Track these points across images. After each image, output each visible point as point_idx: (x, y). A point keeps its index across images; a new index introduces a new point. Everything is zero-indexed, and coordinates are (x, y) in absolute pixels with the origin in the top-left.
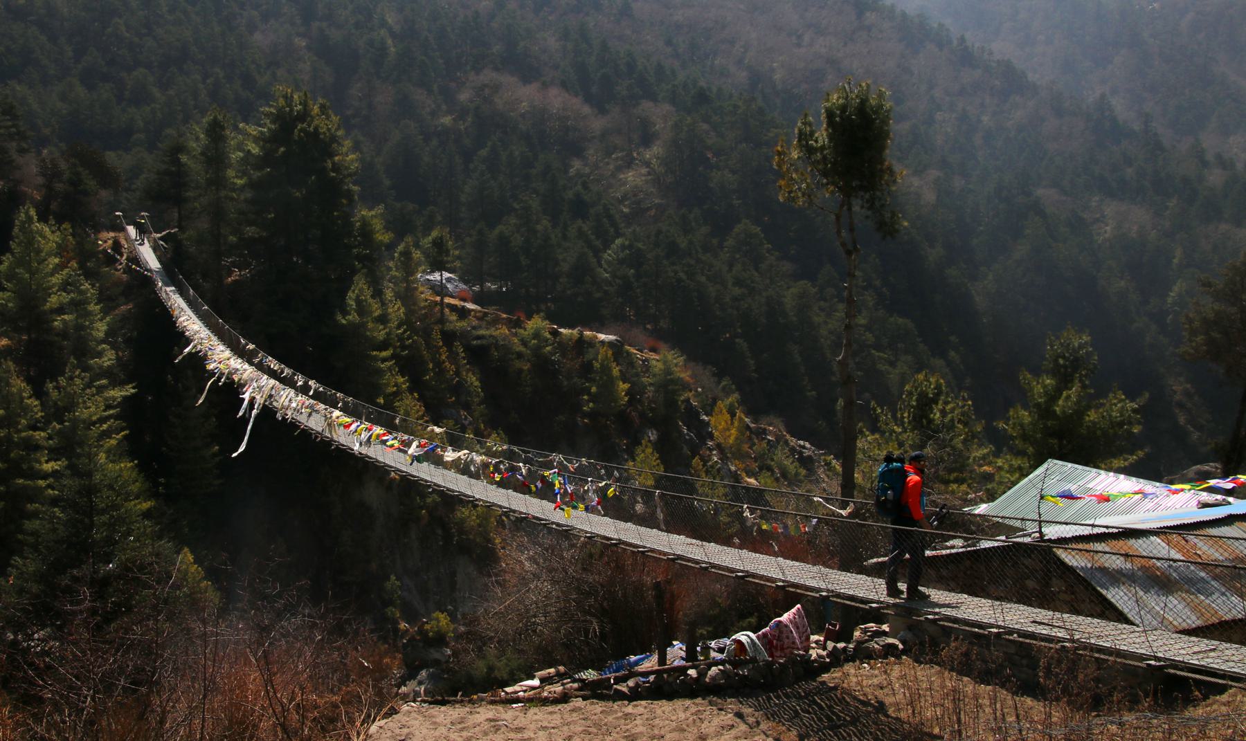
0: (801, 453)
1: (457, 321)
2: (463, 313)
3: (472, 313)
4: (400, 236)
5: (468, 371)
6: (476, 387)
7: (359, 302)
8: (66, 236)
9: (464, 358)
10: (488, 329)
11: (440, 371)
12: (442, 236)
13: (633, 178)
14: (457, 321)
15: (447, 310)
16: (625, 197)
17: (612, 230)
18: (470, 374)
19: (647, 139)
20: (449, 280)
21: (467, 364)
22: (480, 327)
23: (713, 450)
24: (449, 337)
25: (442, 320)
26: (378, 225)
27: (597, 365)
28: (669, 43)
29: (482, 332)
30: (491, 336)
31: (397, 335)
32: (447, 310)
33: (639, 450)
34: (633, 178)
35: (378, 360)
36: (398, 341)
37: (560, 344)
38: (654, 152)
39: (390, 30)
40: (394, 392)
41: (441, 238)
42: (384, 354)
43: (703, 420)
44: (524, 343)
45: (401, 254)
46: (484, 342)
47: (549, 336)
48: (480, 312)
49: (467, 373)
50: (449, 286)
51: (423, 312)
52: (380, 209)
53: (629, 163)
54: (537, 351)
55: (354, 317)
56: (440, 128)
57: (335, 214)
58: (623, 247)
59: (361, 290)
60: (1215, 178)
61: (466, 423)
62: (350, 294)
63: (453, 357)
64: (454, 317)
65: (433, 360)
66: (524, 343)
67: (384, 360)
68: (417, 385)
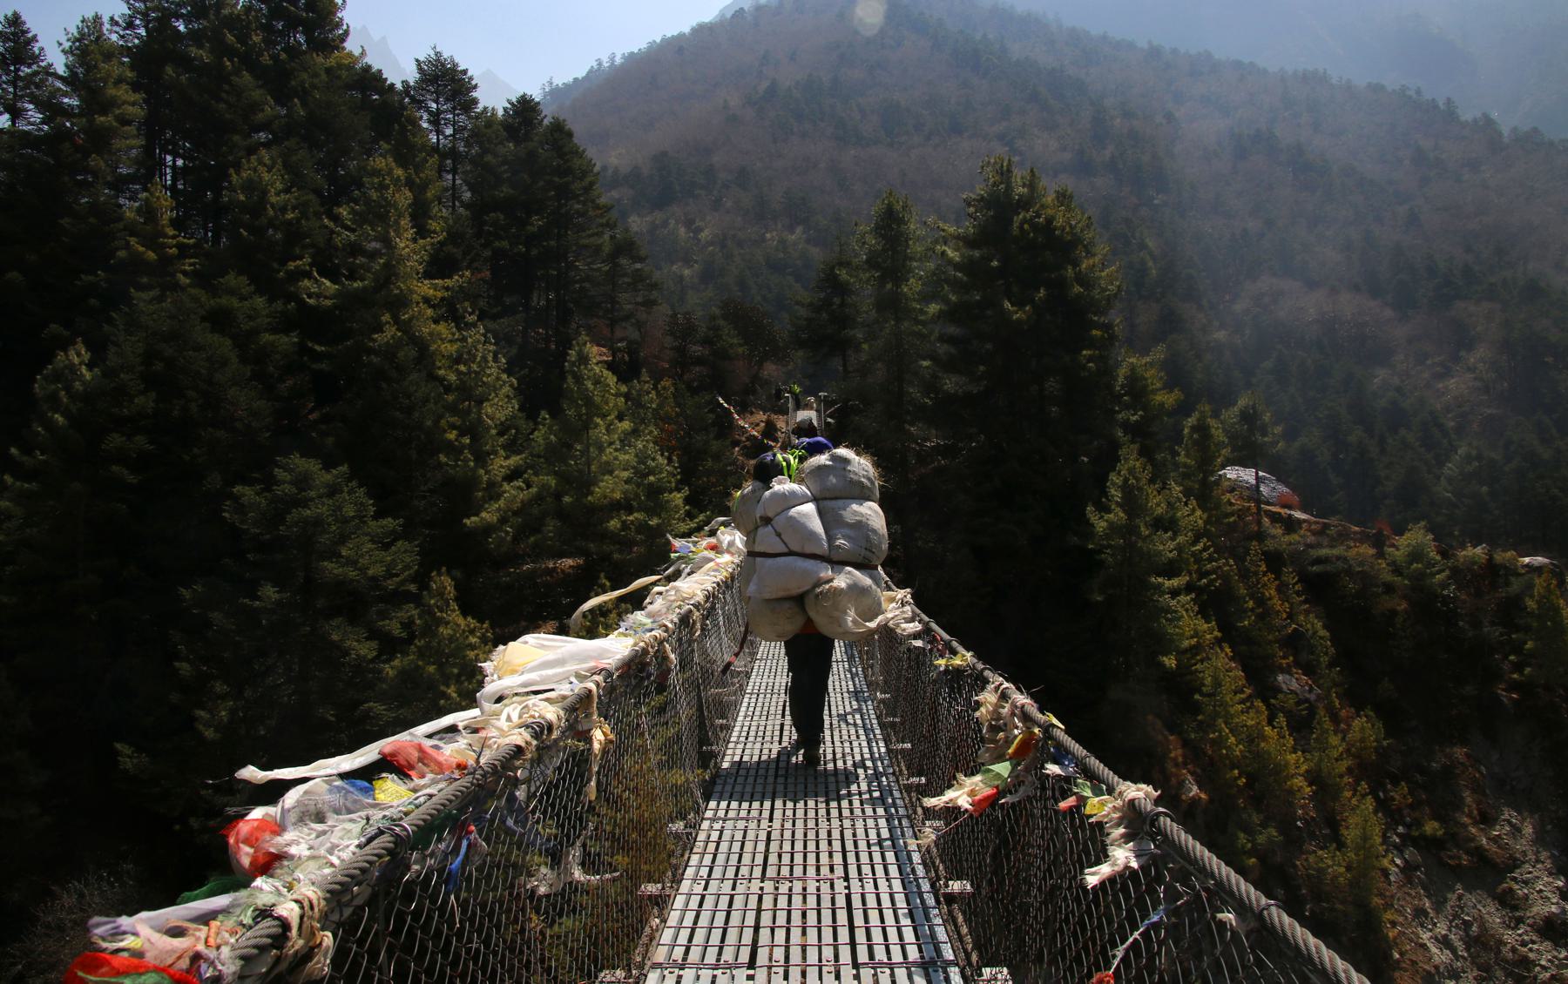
1: (1284, 534)
2: (1290, 525)
3: (1304, 525)
5: (1307, 612)
6: (1321, 638)
7: (1126, 488)
9: (1298, 594)
10: (1332, 547)
11: (1265, 613)
14: (1284, 534)
15: (1266, 521)
21: (1305, 602)
24: (1275, 561)
25: (1260, 536)
26: (1153, 377)
27: (1531, 604)
29: (1324, 552)
30: (1338, 558)
31: (1193, 554)
32: (1266, 521)
34: (1457, 385)
35: (1164, 593)
38: (1479, 356)
40: (1192, 648)
42: (1175, 582)
44: (1397, 570)
45: (1194, 429)
46: (1329, 568)
48: (1317, 523)
51: (1232, 519)
53: (1446, 373)
59: (1131, 471)
61: (1312, 697)
62: (1113, 477)
64: (1277, 531)
65: (1252, 597)
67: (1175, 593)
68: (1229, 633)
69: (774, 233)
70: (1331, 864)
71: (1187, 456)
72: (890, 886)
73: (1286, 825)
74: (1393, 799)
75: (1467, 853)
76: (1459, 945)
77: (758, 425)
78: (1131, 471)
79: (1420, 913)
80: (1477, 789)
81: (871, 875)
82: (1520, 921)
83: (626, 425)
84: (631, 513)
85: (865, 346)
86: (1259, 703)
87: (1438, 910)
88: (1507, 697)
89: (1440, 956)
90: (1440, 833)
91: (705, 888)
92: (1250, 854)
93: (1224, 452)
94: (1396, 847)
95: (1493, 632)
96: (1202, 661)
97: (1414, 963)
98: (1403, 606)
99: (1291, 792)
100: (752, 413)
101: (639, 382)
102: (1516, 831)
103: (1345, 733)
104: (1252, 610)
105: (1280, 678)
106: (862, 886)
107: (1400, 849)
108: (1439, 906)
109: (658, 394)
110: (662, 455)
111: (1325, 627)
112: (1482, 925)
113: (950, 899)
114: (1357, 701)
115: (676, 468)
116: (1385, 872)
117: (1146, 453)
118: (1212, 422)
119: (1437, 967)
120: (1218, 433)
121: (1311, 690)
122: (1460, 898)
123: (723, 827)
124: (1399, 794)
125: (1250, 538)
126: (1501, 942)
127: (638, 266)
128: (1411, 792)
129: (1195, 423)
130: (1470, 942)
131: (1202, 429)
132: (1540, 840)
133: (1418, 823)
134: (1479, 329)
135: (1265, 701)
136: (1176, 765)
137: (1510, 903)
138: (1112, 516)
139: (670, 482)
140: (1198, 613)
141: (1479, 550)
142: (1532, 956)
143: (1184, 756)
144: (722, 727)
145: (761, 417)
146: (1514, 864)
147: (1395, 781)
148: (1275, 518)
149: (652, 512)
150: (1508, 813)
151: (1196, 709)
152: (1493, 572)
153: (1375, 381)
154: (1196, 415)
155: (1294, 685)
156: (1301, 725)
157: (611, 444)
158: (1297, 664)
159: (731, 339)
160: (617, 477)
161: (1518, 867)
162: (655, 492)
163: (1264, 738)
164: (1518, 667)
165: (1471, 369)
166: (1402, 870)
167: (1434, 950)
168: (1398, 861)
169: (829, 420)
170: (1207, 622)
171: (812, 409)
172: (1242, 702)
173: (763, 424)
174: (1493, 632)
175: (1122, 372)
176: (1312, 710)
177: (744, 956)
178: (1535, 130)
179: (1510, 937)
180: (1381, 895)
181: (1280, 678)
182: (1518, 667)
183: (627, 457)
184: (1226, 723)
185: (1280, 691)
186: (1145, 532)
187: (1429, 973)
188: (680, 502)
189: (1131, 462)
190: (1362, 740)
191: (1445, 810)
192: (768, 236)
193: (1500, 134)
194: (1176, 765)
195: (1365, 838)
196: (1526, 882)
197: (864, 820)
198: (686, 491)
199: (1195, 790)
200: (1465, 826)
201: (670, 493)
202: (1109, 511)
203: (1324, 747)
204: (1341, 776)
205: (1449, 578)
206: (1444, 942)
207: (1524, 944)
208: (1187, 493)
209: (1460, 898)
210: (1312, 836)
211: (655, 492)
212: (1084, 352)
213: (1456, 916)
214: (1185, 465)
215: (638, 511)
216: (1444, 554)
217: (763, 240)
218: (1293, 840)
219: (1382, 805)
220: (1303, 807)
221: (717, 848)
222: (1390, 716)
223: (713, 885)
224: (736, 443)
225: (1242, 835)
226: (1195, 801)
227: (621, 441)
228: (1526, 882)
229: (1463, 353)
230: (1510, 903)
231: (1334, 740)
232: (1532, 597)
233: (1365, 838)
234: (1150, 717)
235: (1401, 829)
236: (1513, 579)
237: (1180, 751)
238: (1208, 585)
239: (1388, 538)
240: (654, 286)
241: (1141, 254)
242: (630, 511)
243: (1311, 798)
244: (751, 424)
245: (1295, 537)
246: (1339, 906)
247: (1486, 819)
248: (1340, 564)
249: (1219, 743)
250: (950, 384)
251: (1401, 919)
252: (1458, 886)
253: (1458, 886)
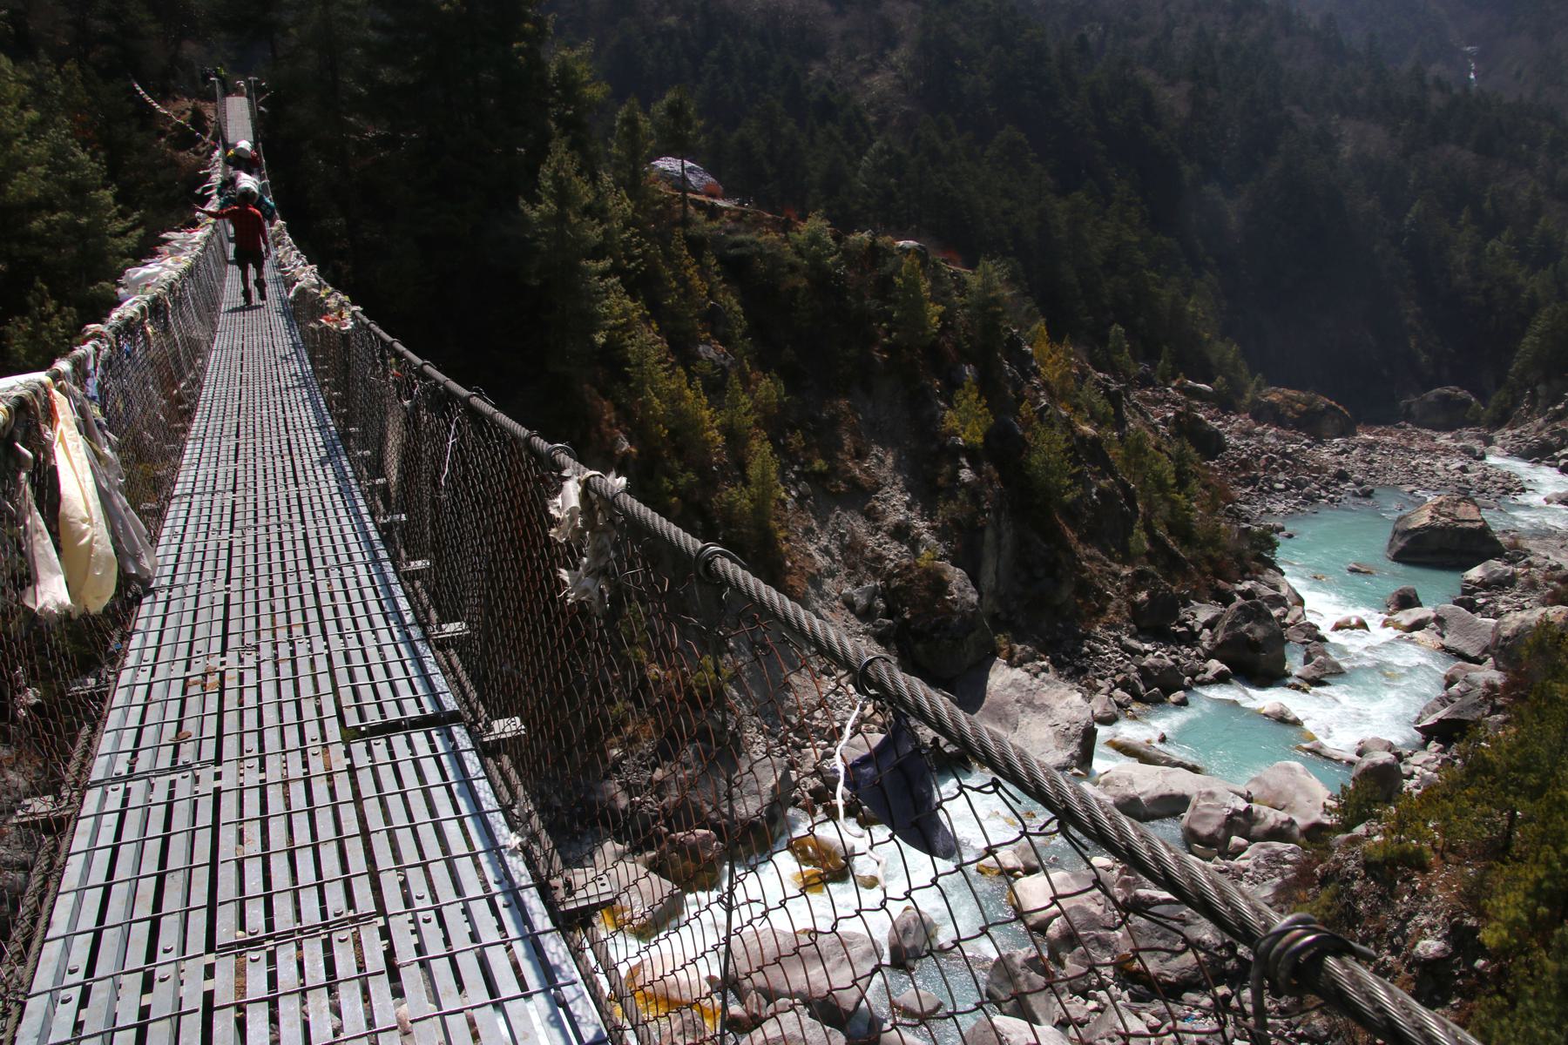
0: (1106, 388)
1: (706, 220)
2: (713, 212)
3: (726, 213)
4: (619, 96)
9: (718, 274)
10: (748, 232)
11: (688, 292)
13: (879, 82)
16: (870, 105)
17: (865, 135)
18: (729, 296)
19: (891, 41)
20: (691, 170)
21: (724, 281)
22: (737, 231)
23: (1040, 390)
24: (696, 246)
25: (686, 222)
26: (583, 71)
27: (898, 281)
29: (741, 237)
30: (752, 242)
33: (959, 395)
34: (879, 82)
36: (623, 250)
37: (846, 253)
38: (900, 55)
43: (1027, 352)
44: (799, 252)
45: (625, 121)
46: (744, 251)
47: (831, 242)
49: (724, 294)
50: (691, 178)
52: (586, 48)
53: (872, 70)
54: (816, 260)
55: (547, 206)
58: (881, 152)
59: (560, 162)
60: (1436, 100)
61: (727, 363)
63: (703, 272)
64: (701, 217)
65: (675, 277)
66: (799, 252)
67: (604, 275)
68: (656, 311)
70: (738, 498)
72: (377, 639)
73: (703, 470)
74: (791, 444)
75: (844, 482)
76: (836, 552)
77: (183, 113)
79: (809, 531)
80: (855, 432)
81: (353, 630)
82: (879, 529)
83: (32, 114)
84: (54, 213)
85: (293, 31)
86: (680, 370)
87: (822, 528)
88: (879, 356)
89: (822, 561)
90: (825, 468)
91: (153, 674)
92: (672, 494)
93: (651, 144)
94: (792, 482)
95: (871, 304)
96: (630, 338)
97: (802, 568)
98: (804, 283)
99: (706, 442)
100: (175, 100)
101: (38, 64)
102: (881, 461)
103: (754, 392)
104: (676, 290)
105: (701, 348)
106: (345, 643)
107: (795, 483)
108: (823, 524)
109: (64, 80)
110: (84, 151)
111: (738, 303)
112: (853, 537)
113: (441, 645)
114: (763, 365)
115: (101, 164)
116: (783, 502)
117: (576, 145)
118: (640, 116)
119: (819, 570)
120: (645, 125)
121: (726, 357)
122: (838, 517)
123: (169, 597)
124: (795, 440)
125: (676, 224)
126: (865, 546)
128: (804, 438)
130: (844, 549)
131: (631, 122)
132: (897, 468)
133: (809, 462)
135: (687, 369)
136: (611, 426)
137: (872, 516)
138: (543, 206)
139: (95, 179)
140: (625, 294)
141: (865, 235)
142: (884, 553)
143: (617, 419)
144: (172, 452)
145: (186, 104)
146: (878, 487)
147: (793, 429)
148: (700, 206)
149: (78, 210)
150: (876, 450)
151: (626, 378)
152: (875, 254)
155: (712, 354)
156: (715, 388)
157: (19, 135)
158: (715, 336)
160: (31, 173)
161: (879, 489)
163: (683, 398)
164: (888, 333)
165: (894, 68)
166: (797, 500)
167: (818, 557)
168: (793, 493)
169: (262, 108)
170: (635, 301)
171: (241, 94)
172: (665, 370)
173: (189, 113)
174: (871, 304)
175: (553, 68)
176: (725, 372)
177: (209, 752)
179: (871, 542)
180: (778, 519)
181: (701, 348)
182: (888, 333)
183: (41, 149)
184: (653, 389)
185: (700, 358)
186: (574, 220)
187: (812, 574)
188: (110, 200)
189: (560, 158)
190: (767, 398)
191: (830, 449)
194: (611, 426)
195: (764, 475)
196: (884, 500)
197: (340, 569)
198: (114, 188)
199: (626, 446)
200: (843, 461)
201: (97, 190)
202: (541, 202)
203: (735, 405)
204: (749, 428)
205: (841, 258)
206: (826, 551)
207: (880, 546)
208: (619, 183)
209: (838, 517)
210: (725, 477)
212: (515, 45)
213: (835, 531)
214: (618, 157)
215: (62, 210)
216: (837, 238)
218: (709, 482)
219: (778, 449)
220: (717, 454)
221: (160, 639)
222: (791, 377)
223: (162, 671)
224: (162, 134)
225: (665, 480)
226: (627, 454)
227: (28, 133)
228: (884, 500)
229: (887, 52)
230: (872, 516)
231: (744, 398)
232: (900, 275)
233: (764, 475)
234: (586, 386)
235: (796, 468)
236: (888, 259)
237: (613, 414)
238: (635, 269)
239: (795, 224)
242: (53, 209)
243: (724, 447)
244: (176, 112)
245: (716, 224)
246: (744, 530)
247: (860, 455)
248: (754, 248)
249: (646, 405)
250: (386, 74)
251: (794, 537)
252: (837, 508)
253: (837, 508)
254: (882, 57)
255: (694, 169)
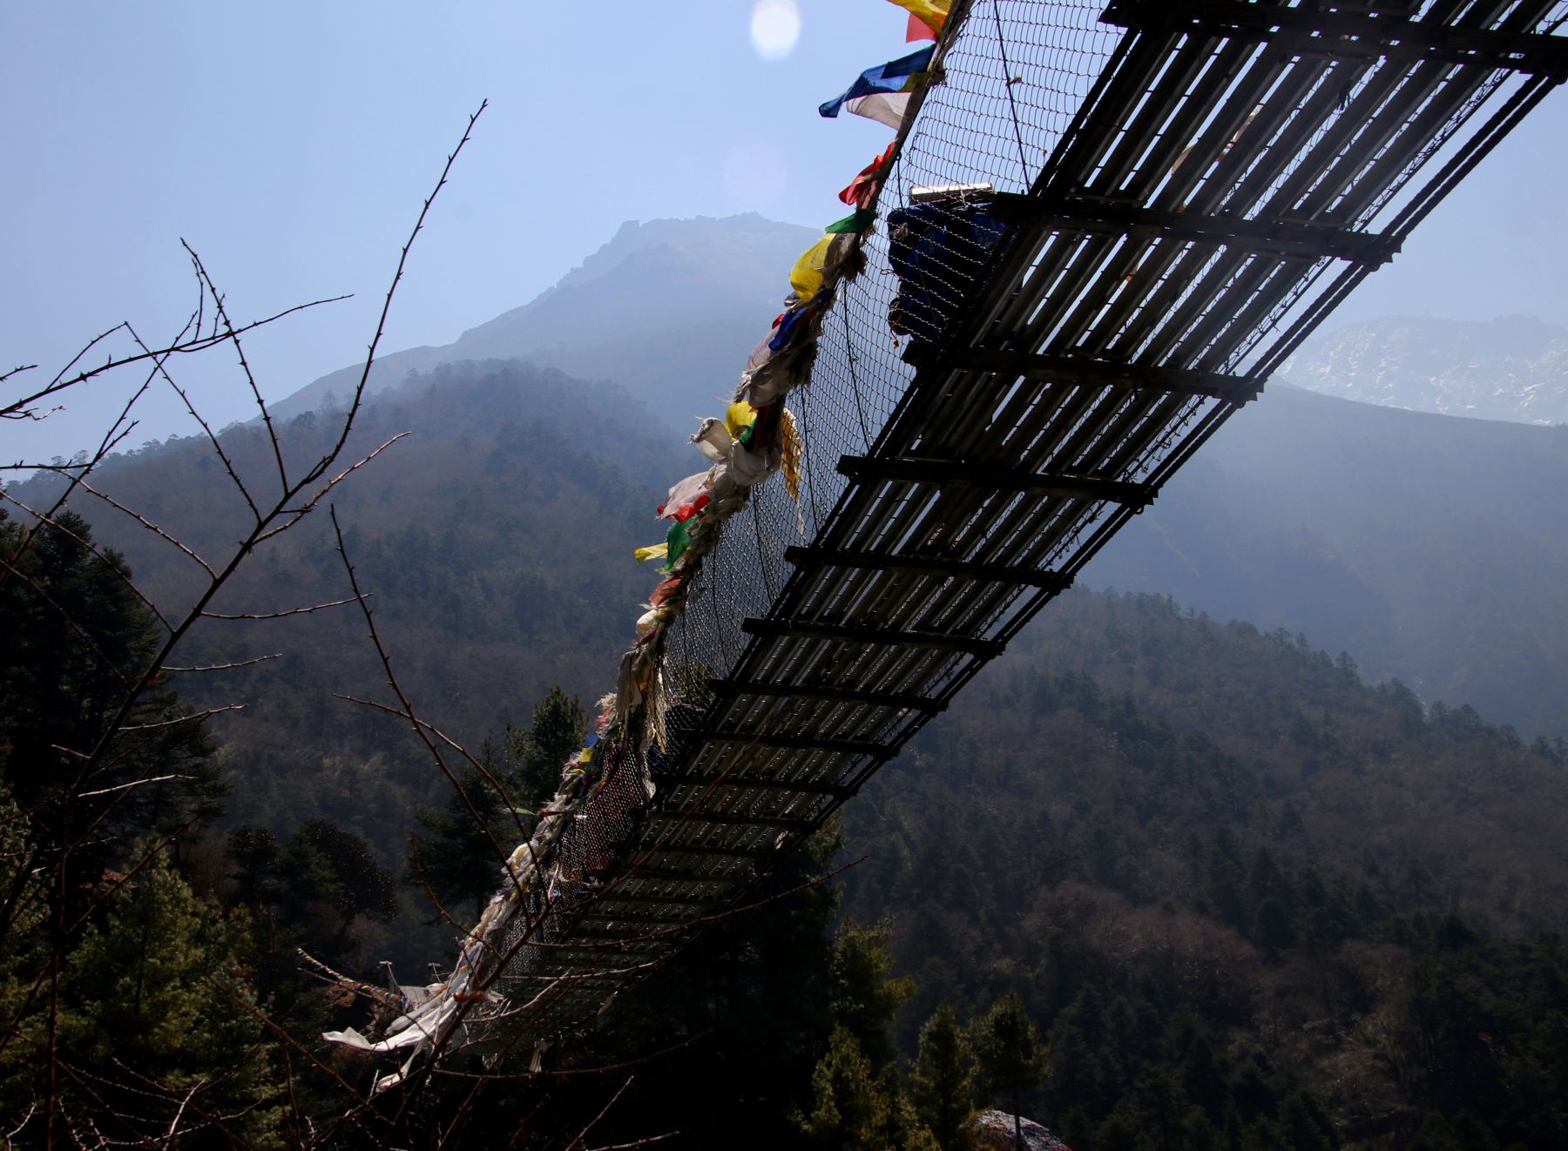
7: (839, 1081)
8: (240, 931)
12: (1014, 1013)
17: (1326, 1140)
19: (1364, 1002)
20: (1030, 1131)
28: (1372, 871)
38: (1380, 1023)
39: (906, 837)
41: (1013, 1016)
56: (991, 977)
57: (793, 912)
59: (846, 1060)
69: (338, 759)
71: (924, 1073)
78: (846, 1060)
127: (199, 760)
129: (935, 1028)
131: (943, 1038)
134: (1379, 982)
153: (1230, 1047)
154: (935, 1018)
159: (320, 868)
162: (236, 1039)
165: (1370, 1043)
175: (840, 944)
178: (1467, 709)
192: (327, 762)
193: (1418, 710)
211: (236, 1039)
214: (923, 1087)
217: (319, 768)
229: (1356, 1016)
240: (219, 791)
241: (893, 837)
254: (1349, 1025)
255: (1035, 1128)
